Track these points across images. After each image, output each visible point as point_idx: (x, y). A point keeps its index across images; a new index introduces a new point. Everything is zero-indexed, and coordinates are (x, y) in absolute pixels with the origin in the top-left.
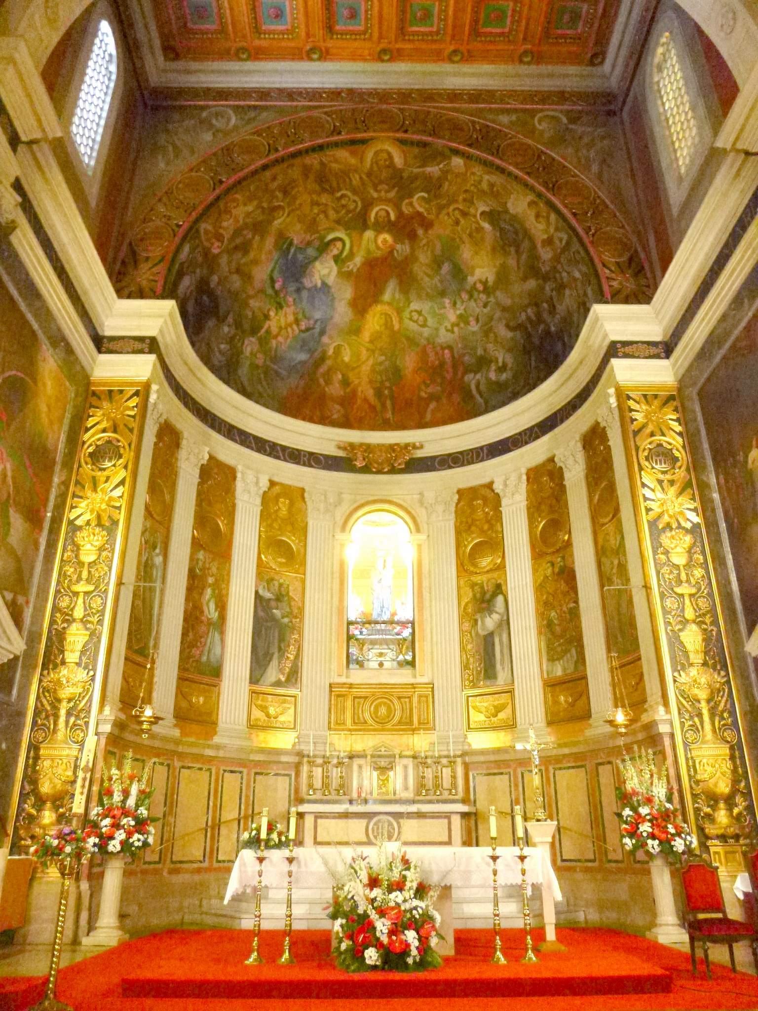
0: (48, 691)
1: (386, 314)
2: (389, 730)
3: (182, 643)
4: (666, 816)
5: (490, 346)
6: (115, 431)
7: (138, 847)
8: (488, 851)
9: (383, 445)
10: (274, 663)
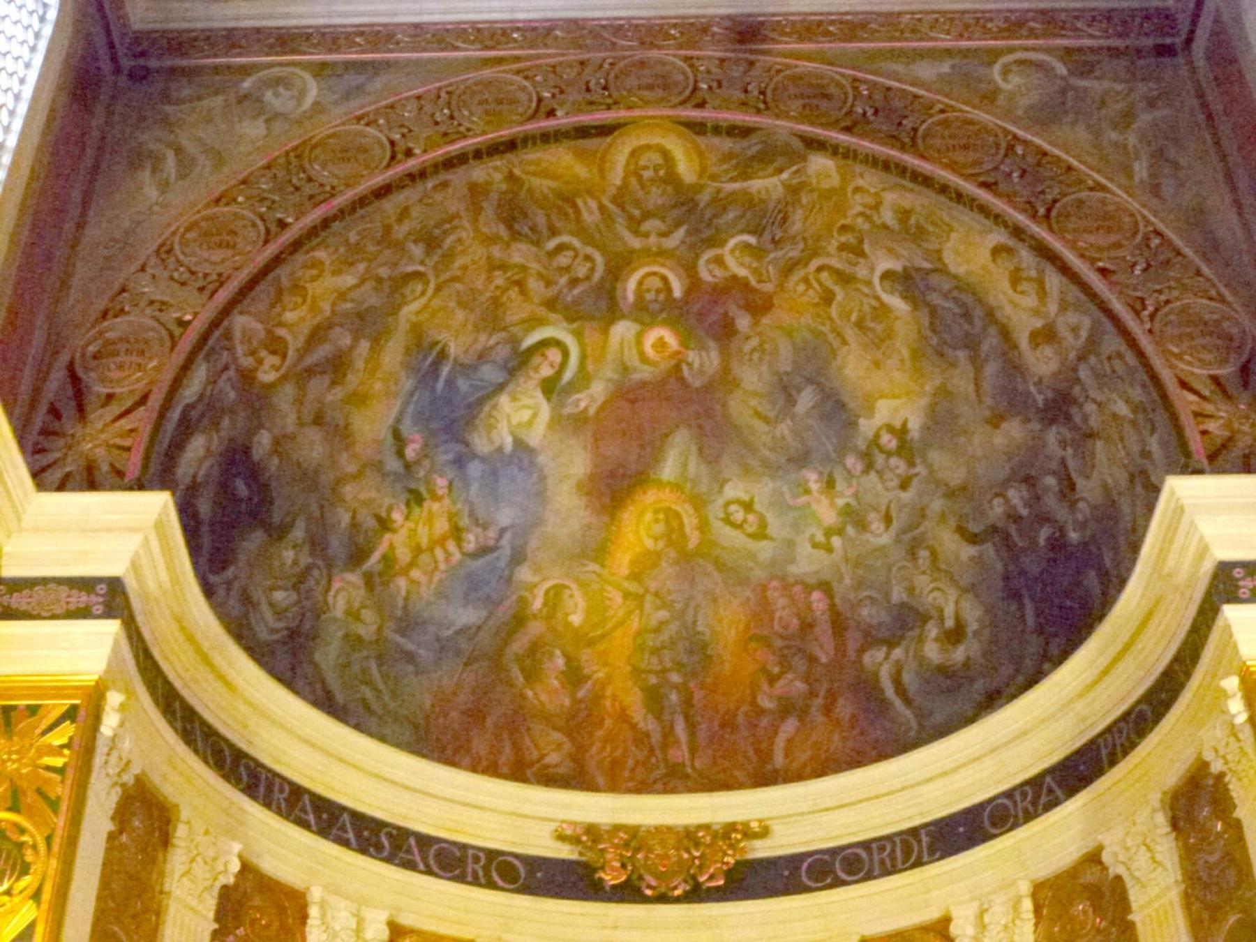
1: (668, 511)
6: (14, 808)
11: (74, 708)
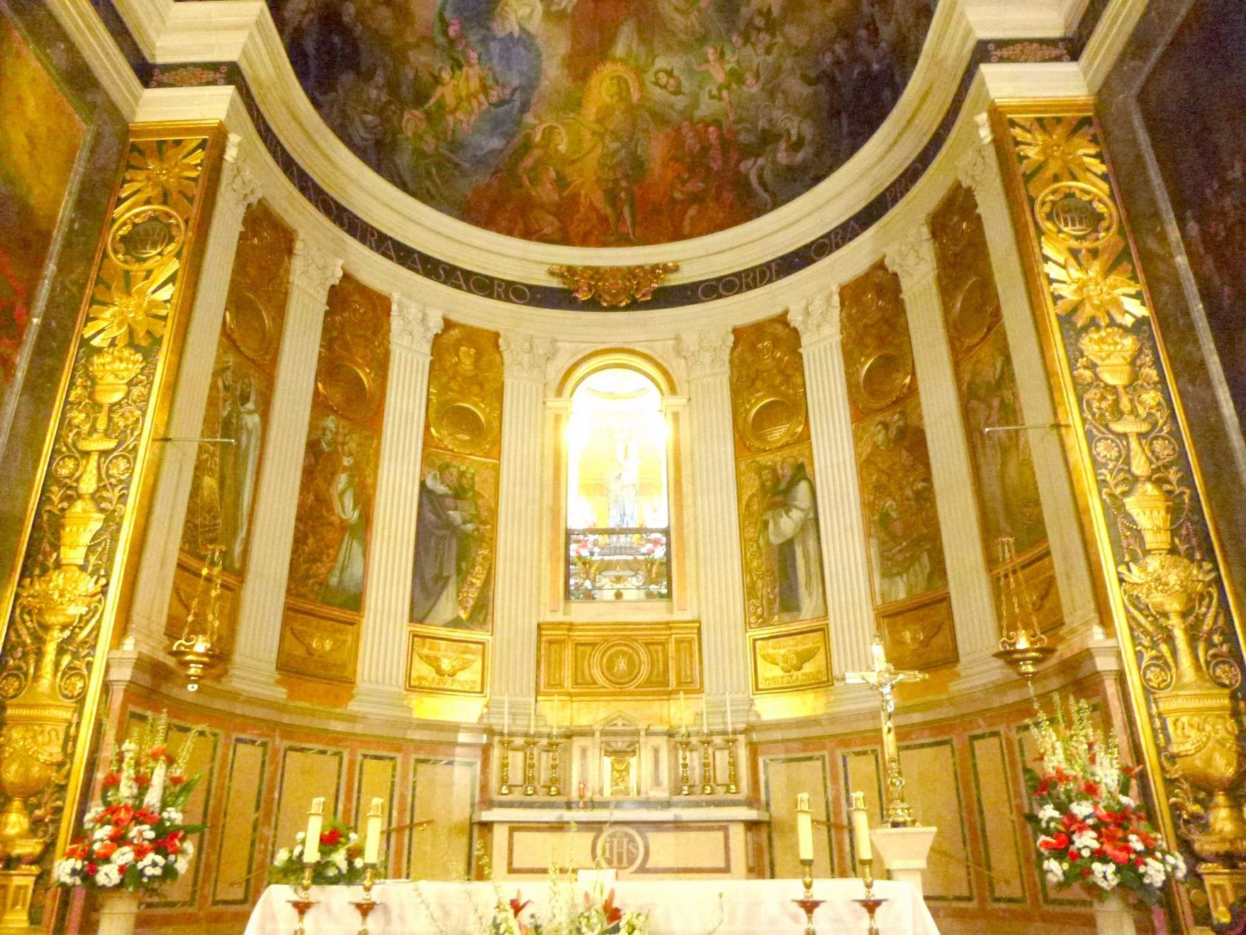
0: (30, 613)
1: (619, 78)
2: (631, 694)
3: (294, 552)
4: (1121, 818)
5: (778, 114)
6: (165, 203)
7: (152, 878)
9: (618, 269)
10: (451, 589)
11: (205, 141)
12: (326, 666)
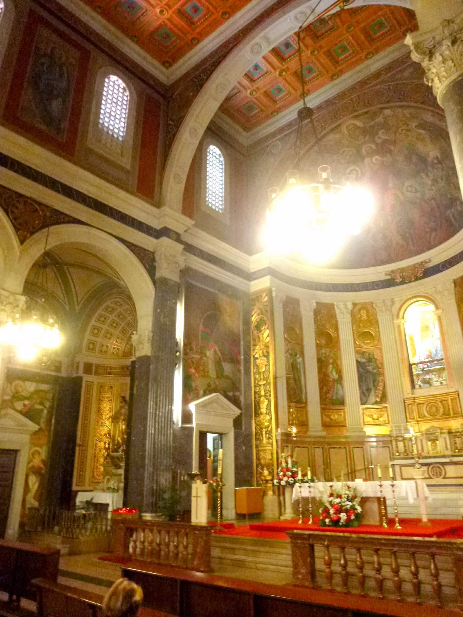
2: (438, 419)
8: (378, 483)
10: (372, 393)
12: (338, 423)
